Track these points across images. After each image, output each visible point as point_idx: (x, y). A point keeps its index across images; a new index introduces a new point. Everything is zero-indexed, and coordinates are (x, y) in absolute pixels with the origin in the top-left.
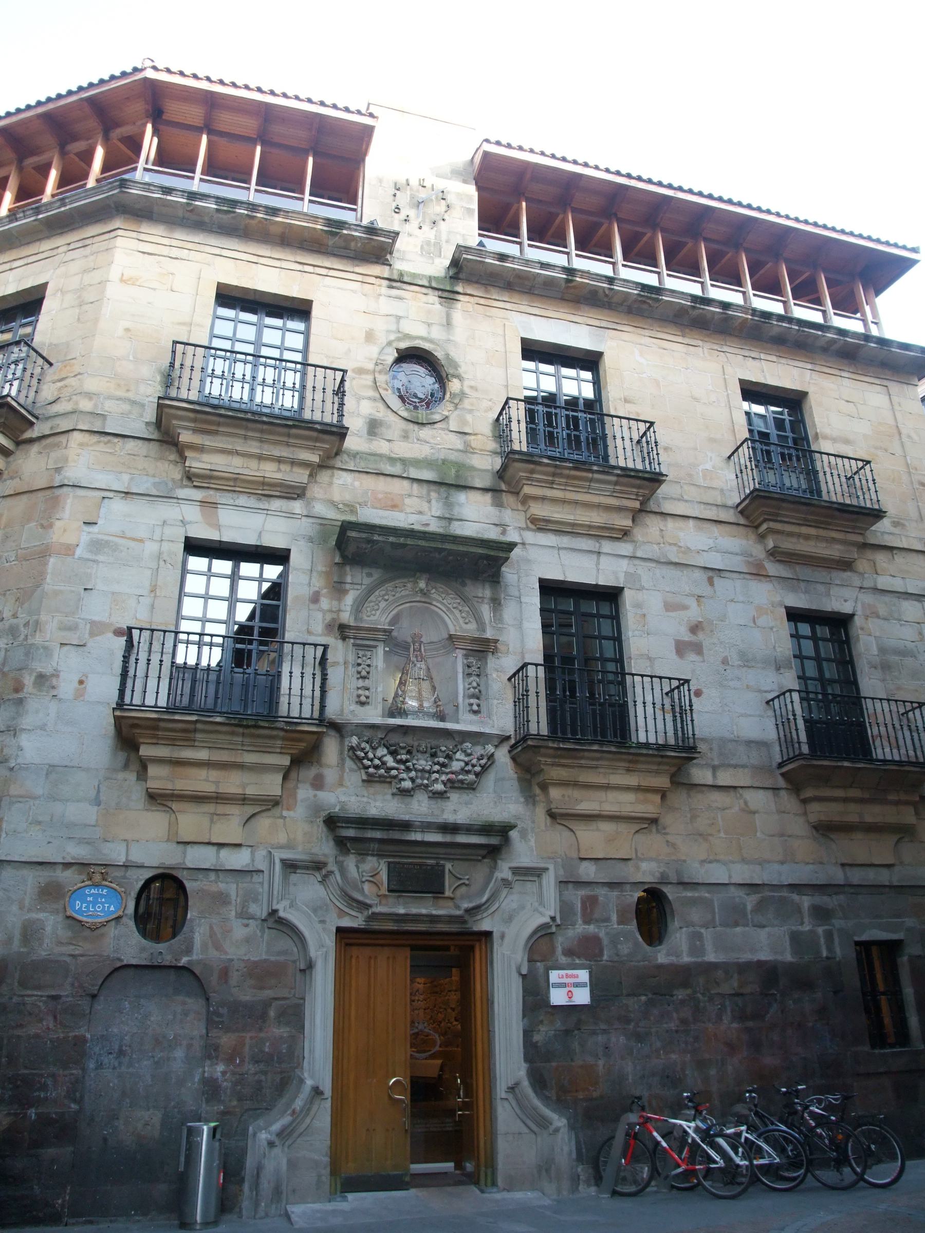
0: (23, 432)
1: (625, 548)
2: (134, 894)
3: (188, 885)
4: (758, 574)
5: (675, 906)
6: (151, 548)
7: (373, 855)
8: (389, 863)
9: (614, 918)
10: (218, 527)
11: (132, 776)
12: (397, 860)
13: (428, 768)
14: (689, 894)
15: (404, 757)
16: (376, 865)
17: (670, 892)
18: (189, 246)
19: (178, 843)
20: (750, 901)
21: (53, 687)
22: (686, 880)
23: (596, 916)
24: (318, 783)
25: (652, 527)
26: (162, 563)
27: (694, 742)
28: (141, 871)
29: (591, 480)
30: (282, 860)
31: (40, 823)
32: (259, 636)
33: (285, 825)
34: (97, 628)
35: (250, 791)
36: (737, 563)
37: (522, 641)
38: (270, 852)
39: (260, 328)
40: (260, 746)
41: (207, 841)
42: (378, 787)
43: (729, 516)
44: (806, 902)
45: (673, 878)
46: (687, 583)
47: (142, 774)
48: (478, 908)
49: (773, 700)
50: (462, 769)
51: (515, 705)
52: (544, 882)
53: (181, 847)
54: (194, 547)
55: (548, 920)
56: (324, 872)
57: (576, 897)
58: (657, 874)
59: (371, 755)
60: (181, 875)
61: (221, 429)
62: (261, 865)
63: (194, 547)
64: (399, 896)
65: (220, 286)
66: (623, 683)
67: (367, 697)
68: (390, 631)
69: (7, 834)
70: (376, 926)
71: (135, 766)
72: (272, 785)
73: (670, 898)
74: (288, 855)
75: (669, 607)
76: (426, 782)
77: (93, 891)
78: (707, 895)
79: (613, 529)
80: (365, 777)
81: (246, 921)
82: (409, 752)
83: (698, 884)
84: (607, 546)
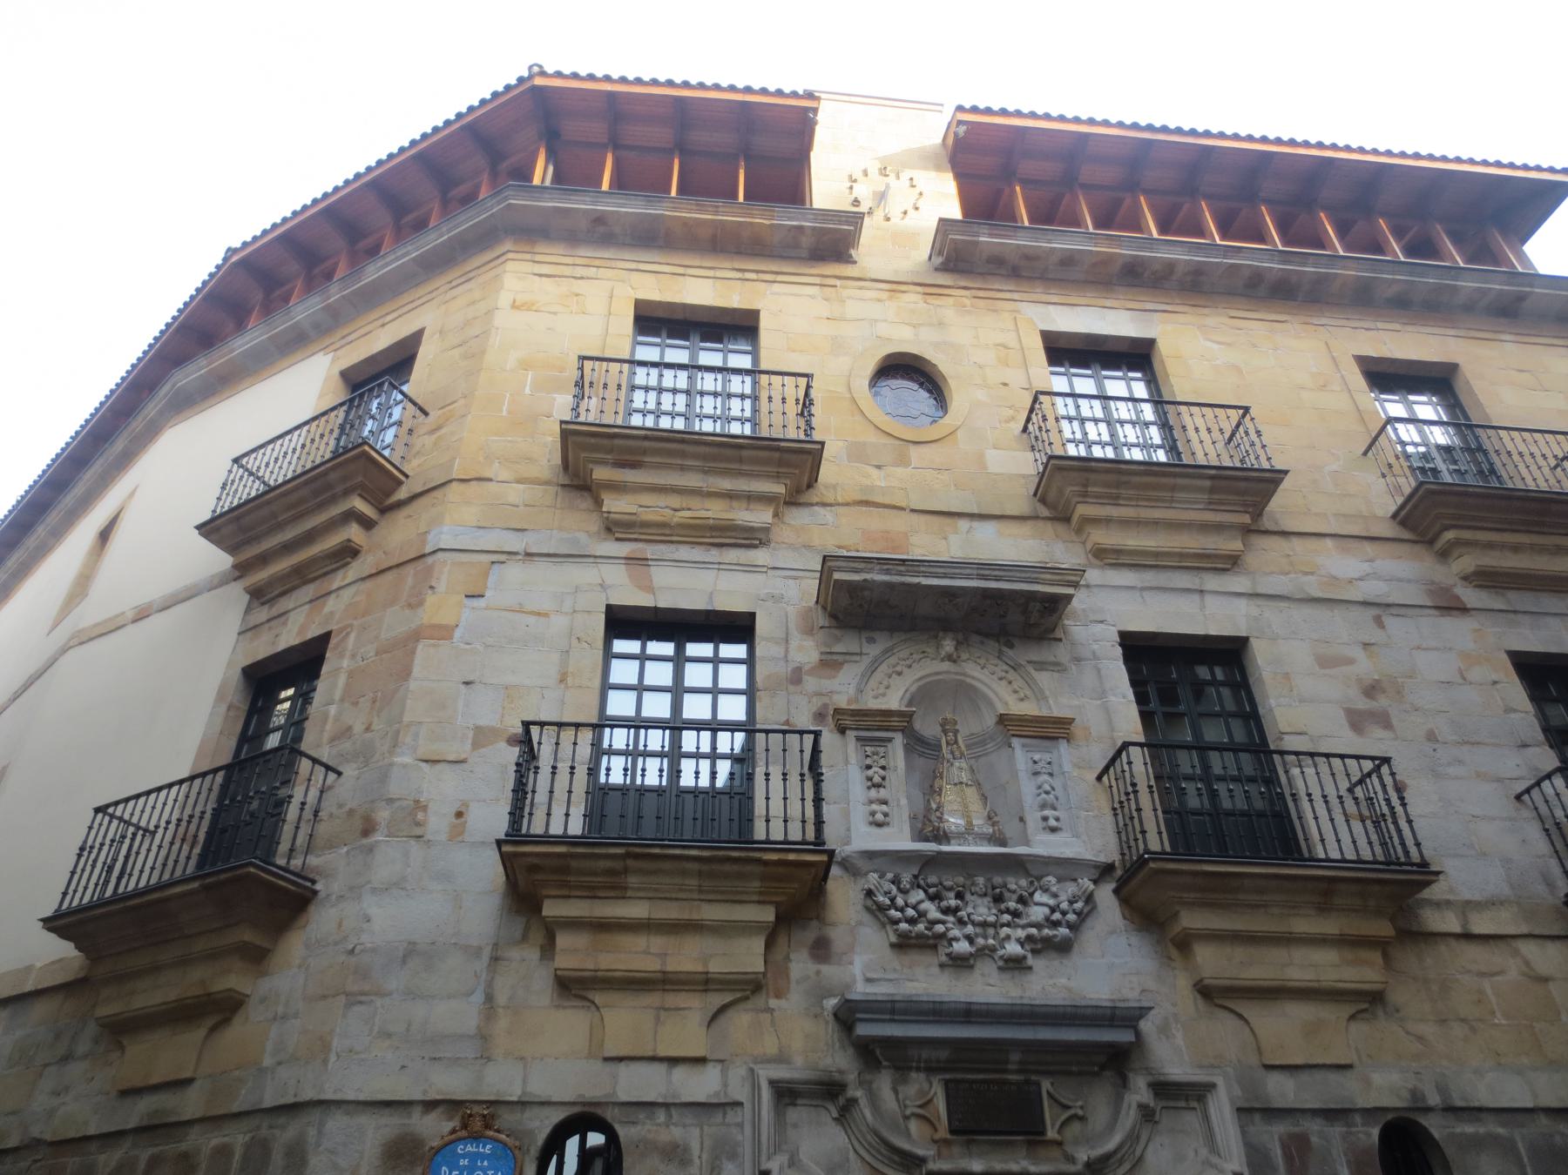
0: (389, 494)
2: (534, 1152)
4: (1451, 607)
5: (1450, 1151)
6: (559, 623)
7: (918, 1069)
8: (947, 1083)
10: (650, 589)
11: (532, 954)
12: (959, 1076)
13: (992, 919)
14: (1469, 1129)
15: (953, 903)
16: (926, 1086)
17: (1436, 1127)
18: (597, 263)
19: (607, 1059)
21: (418, 824)
22: (1459, 1103)
24: (821, 950)
25: (1266, 552)
26: (575, 641)
28: (546, 1111)
29: (1173, 488)
30: (772, 1083)
31: (389, 1035)
33: (773, 1023)
34: (482, 737)
35: (716, 967)
37: (1110, 721)
38: (752, 1070)
39: (679, 660)
40: (723, 892)
41: (650, 1054)
42: (915, 956)
43: (1388, 530)
45: (1434, 1099)
46: (1343, 629)
47: (548, 949)
48: (1107, 1157)
49: (1528, 791)
50: (1047, 919)
51: (1116, 815)
52: (1212, 1111)
53: (611, 1067)
54: (622, 622)
56: (841, 1101)
57: (1272, 1135)
58: (1406, 1094)
59: (900, 901)
62: (739, 1092)
63: (622, 622)
64: (969, 1143)
65: (639, 304)
66: (1271, 780)
67: (886, 815)
68: (910, 715)
69: (338, 1056)
71: (538, 936)
72: (748, 956)
73: (1436, 1135)
74: (781, 1073)
75: (1325, 662)
76: (991, 941)
77: (469, 1148)
78: (1501, 1130)
79: (1216, 556)
80: (893, 939)
82: (959, 896)
83: (1480, 1109)
84: (1212, 582)
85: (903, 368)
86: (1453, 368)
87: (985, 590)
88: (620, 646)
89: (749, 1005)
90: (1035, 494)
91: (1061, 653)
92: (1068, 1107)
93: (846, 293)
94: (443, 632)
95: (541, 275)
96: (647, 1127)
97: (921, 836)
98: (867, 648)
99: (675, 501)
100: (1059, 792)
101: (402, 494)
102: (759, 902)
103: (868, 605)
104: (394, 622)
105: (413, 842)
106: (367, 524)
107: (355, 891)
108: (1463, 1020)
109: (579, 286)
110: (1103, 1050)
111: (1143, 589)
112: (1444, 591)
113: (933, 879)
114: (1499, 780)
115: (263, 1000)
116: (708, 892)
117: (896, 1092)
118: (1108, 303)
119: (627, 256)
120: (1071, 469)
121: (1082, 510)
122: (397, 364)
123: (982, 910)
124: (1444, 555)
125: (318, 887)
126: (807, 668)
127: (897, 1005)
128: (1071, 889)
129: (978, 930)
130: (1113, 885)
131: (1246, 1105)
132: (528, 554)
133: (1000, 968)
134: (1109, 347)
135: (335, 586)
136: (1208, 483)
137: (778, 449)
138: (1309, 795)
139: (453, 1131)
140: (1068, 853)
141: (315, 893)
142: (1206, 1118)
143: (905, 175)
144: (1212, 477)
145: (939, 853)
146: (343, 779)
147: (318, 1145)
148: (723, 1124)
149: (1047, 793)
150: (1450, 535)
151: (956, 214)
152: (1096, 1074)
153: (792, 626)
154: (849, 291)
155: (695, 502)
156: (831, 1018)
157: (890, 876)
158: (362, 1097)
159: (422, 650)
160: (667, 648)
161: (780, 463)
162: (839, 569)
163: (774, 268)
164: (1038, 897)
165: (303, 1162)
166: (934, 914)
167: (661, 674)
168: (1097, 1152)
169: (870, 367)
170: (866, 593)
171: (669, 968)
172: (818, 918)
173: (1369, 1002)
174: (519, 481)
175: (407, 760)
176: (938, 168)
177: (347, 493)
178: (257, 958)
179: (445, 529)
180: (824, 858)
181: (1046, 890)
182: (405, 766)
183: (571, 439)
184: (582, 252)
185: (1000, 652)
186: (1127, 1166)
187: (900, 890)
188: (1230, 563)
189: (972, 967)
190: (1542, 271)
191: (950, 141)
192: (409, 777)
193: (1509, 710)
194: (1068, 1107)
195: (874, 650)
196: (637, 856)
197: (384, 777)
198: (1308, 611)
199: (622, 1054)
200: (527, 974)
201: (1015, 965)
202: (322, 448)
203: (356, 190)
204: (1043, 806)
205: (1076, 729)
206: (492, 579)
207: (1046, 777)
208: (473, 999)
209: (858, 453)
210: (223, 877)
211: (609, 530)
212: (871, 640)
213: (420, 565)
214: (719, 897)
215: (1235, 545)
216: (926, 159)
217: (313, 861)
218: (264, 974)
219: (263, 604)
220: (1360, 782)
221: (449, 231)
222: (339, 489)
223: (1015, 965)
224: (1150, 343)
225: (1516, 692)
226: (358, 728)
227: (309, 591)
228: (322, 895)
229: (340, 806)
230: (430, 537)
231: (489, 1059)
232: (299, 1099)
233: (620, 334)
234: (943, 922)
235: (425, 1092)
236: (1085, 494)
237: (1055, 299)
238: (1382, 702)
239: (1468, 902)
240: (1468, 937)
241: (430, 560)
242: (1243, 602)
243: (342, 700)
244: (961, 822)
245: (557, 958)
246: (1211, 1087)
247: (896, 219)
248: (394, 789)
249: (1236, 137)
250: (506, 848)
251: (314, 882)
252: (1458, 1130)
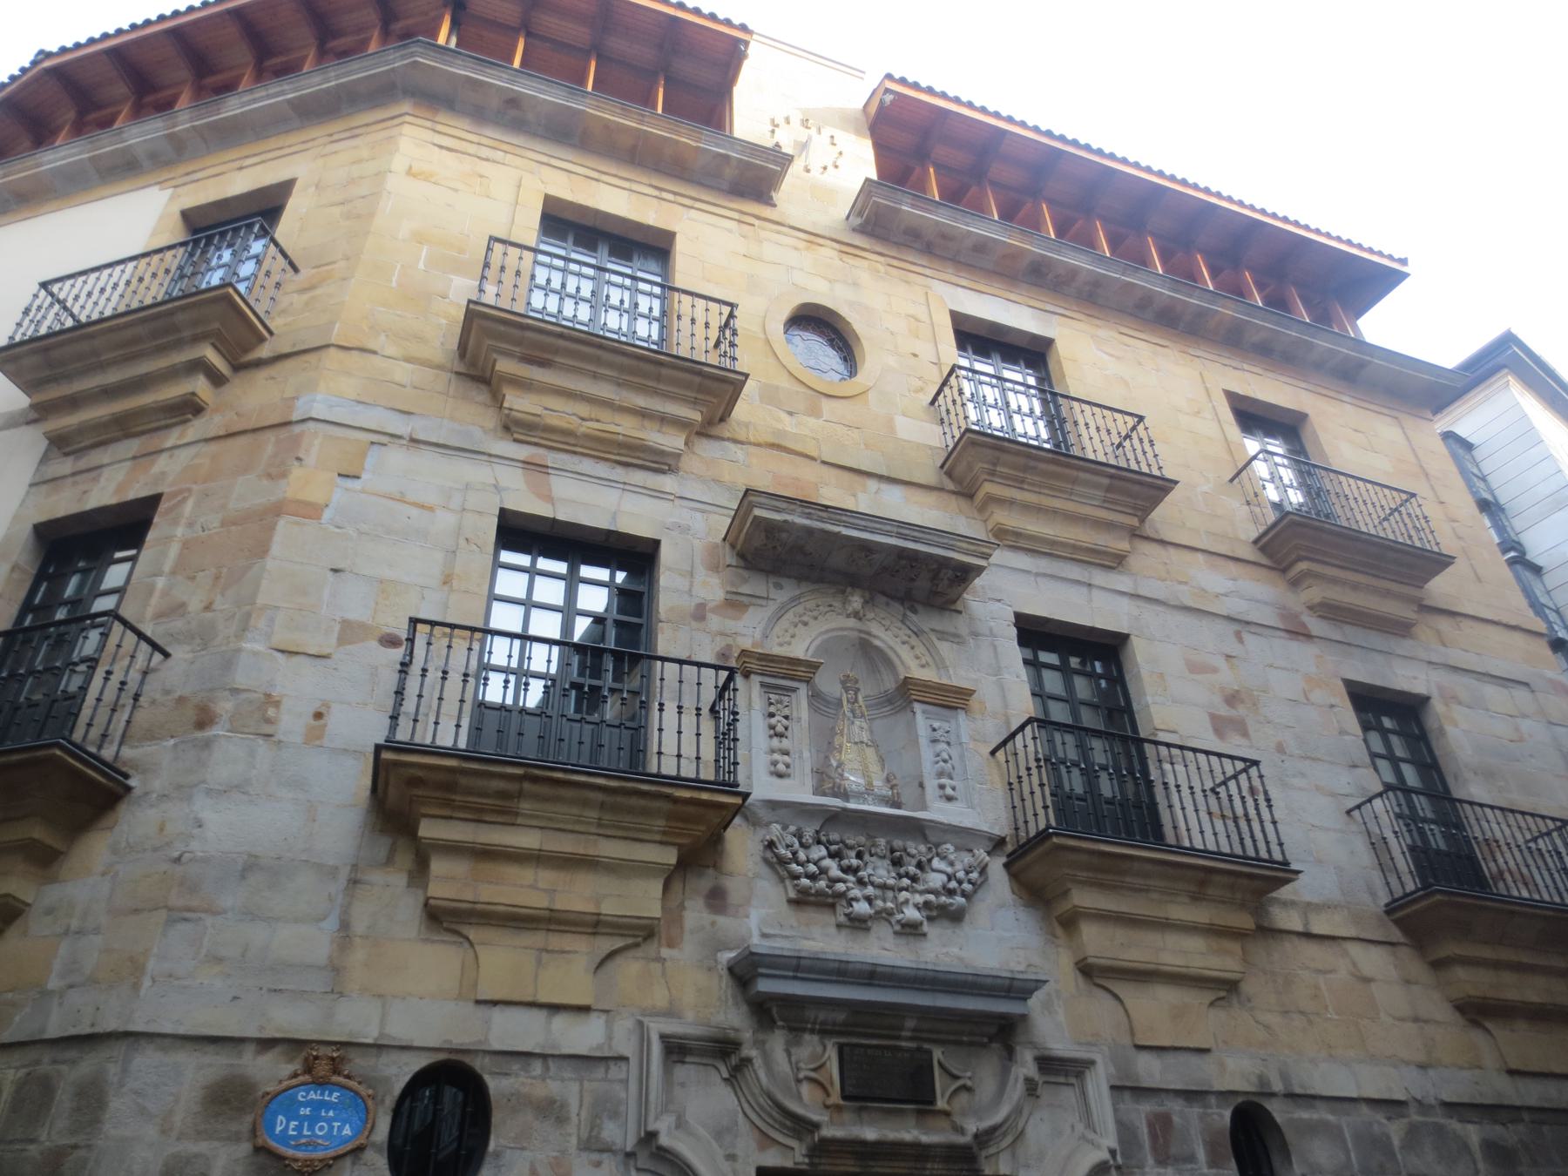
0: (246, 351)
1: (1121, 582)
3: (494, 1085)
4: (1299, 633)
5: (1290, 1135)
7: (812, 1031)
8: (841, 1049)
9: (1201, 1154)
10: (549, 499)
12: (855, 1040)
13: (891, 882)
15: (855, 862)
16: (819, 1049)
17: (1279, 1111)
18: (505, 147)
19: (478, 1002)
20: (1395, 1131)
22: (1298, 1090)
23: (1173, 1150)
24: (717, 899)
25: (1146, 558)
26: (462, 542)
27: (1283, 853)
28: (406, 1057)
29: (1075, 481)
30: (663, 1037)
31: (219, 960)
32: (613, 658)
33: (664, 973)
34: (350, 632)
35: (609, 908)
36: (1268, 617)
38: (641, 1023)
41: (530, 999)
44: (1473, 1134)
45: (1277, 1086)
46: (1211, 639)
47: (420, 871)
50: (944, 887)
53: (483, 1010)
54: (519, 533)
55: (1105, 1155)
56: (734, 1060)
57: (1140, 1113)
58: (1254, 1079)
59: (802, 856)
60: (478, 1064)
61: (558, 359)
62: (625, 1045)
63: (519, 533)
64: (861, 1109)
70: (825, 1165)
71: (405, 860)
72: (645, 899)
73: (1278, 1118)
76: (890, 905)
77: (312, 1096)
78: (1331, 1118)
79: (1105, 553)
80: (792, 894)
81: (595, 1156)
82: (859, 856)
84: (1099, 577)
85: (815, 320)
86: (1302, 417)
87: (904, 549)
88: (507, 557)
89: (639, 953)
90: (942, 467)
91: (960, 625)
92: (956, 1078)
93: (763, 234)
94: (311, 511)
95: (441, 147)
96: (521, 1079)
97: (818, 791)
98: (774, 593)
99: (583, 409)
100: (956, 761)
101: (264, 352)
102: (661, 843)
103: (782, 549)
104: (247, 492)
105: (261, 741)
106: (217, 380)
107: (183, 791)
108: (1302, 1013)
109: (485, 168)
110: (989, 1022)
111: (1037, 575)
112: (1294, 617)
113: (835, 836)
114: (1333, 795)
115: (50, 911)
116: (606, 826)
117: (789, 1055)
118: (1013, 297)
119: (539, 147)
120: (984, 445)
121: (989, 488)
122: (264, 209)
123: (881, 872)
124: (1295, 583)
125: (132, 782)
126: (711, 605)
127: (803, 962)
128: (967, 859)
129: (878, 892)
130: (1004, 860)
131: (1119, 1083)
132: (413, 441)
133: (896, 933)
134: (1008, 339)
135: (169, 444)
136: (1106, 481)
137: (700, 373)
138: (1178, 786)
139: (295, 1075)
140: (967, 823)
141: (129, 789)
142: (1084, 1094)
143: (828, 131)
144: (1111, 477)
145: (845, 810)
146: (170, 662)
147: (121, 1085)
148: (605, 1080)
149: (945, 761)
150: (1303, 566)
151: (874, 176)
152: (983, 1046)
153: (698, 560)
154: (767, 232)
155: (605, 415)
156: (725, 973)
157: (792, 828)
158: (182, 1031)
159: (283, 525)
160: (561, 567)
161: (701, 389)
162: (761, 506)
163: (693, 194)
164: (936, 863)
165: (101, 1104)
166: (835, 872)
167: (551, 591)
168: (986, 1124)
169: (786, 313)
170: (784, 535)
171: (558, 906)
172: (715, 866)
173: (1226, 989)
174: (408, 360)
175: (259, 647)
176: (858, 132)
177: (196, 339)
178: (46, 860)
179: (319, 397)
180: (738, 801)
181: (943, 858)
182: (255, 654)
183: (476, 322)
184: (489, 132)
185: (904, 615)
186: (1009, 1139)
187: (802, 845)
188: (1115, 562)
189: (868, 929)
190: (1368, 340)
191: (873, 109)
192: (256, 666)
193: (1342, 732)
194: (956, 1078)
195: (781, 596)
196: (535, 780)
197: (228, 663)
198: (1180, 617)
199: (497, 997)
200: (391, 900)
201: (911, 930)
202: (102, 302)
203: (155, 35)
204: (940, 774)
205: (974, 702)
206: (370, 461)
207: (945, 746)
208: (324, 924)
209: (770, 396)
210: (15, 757)
211: (507, 428)
212: (779, 586)
213: (283, 433)
214: (620, 833)
215: (1123, 545)
216: (846, 120)
217: (127, 752)
218: (53, 880)
219: (67, 454)
220: (1224, 783)
221: (337, 77)
222: (187, 333)
223: (911, 930)
224: (1049, 342)
225: (1348, 717)
226: (195, 605)
227: (133, 446)
228: (137, 792)
229: (167, 692)
230: (299, 403)
231: (341, 994)
232: (98, 1029)
233: (528, 227)
234: (844, 881)
235: (262, 1028)
236: (993, 473)
237: (964, 282)
238: (1241, 711)
239: (1309, 904)
240: (1308, 935)
241: (297, 429)
242: (1125, 601)
243: (173, 573)
244: (861, 781)
245: (431, 886)
246: (1091, 1063)
247: (816, 172)
248: (240, 679)
249: (1136, 165)
250: (386, 755)
251: (127, 776)
252: (1296, 1116)
